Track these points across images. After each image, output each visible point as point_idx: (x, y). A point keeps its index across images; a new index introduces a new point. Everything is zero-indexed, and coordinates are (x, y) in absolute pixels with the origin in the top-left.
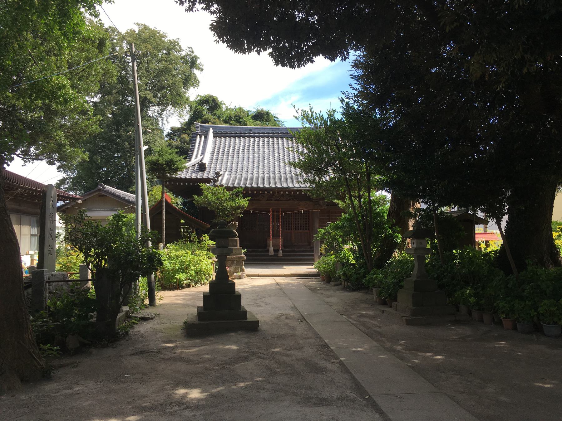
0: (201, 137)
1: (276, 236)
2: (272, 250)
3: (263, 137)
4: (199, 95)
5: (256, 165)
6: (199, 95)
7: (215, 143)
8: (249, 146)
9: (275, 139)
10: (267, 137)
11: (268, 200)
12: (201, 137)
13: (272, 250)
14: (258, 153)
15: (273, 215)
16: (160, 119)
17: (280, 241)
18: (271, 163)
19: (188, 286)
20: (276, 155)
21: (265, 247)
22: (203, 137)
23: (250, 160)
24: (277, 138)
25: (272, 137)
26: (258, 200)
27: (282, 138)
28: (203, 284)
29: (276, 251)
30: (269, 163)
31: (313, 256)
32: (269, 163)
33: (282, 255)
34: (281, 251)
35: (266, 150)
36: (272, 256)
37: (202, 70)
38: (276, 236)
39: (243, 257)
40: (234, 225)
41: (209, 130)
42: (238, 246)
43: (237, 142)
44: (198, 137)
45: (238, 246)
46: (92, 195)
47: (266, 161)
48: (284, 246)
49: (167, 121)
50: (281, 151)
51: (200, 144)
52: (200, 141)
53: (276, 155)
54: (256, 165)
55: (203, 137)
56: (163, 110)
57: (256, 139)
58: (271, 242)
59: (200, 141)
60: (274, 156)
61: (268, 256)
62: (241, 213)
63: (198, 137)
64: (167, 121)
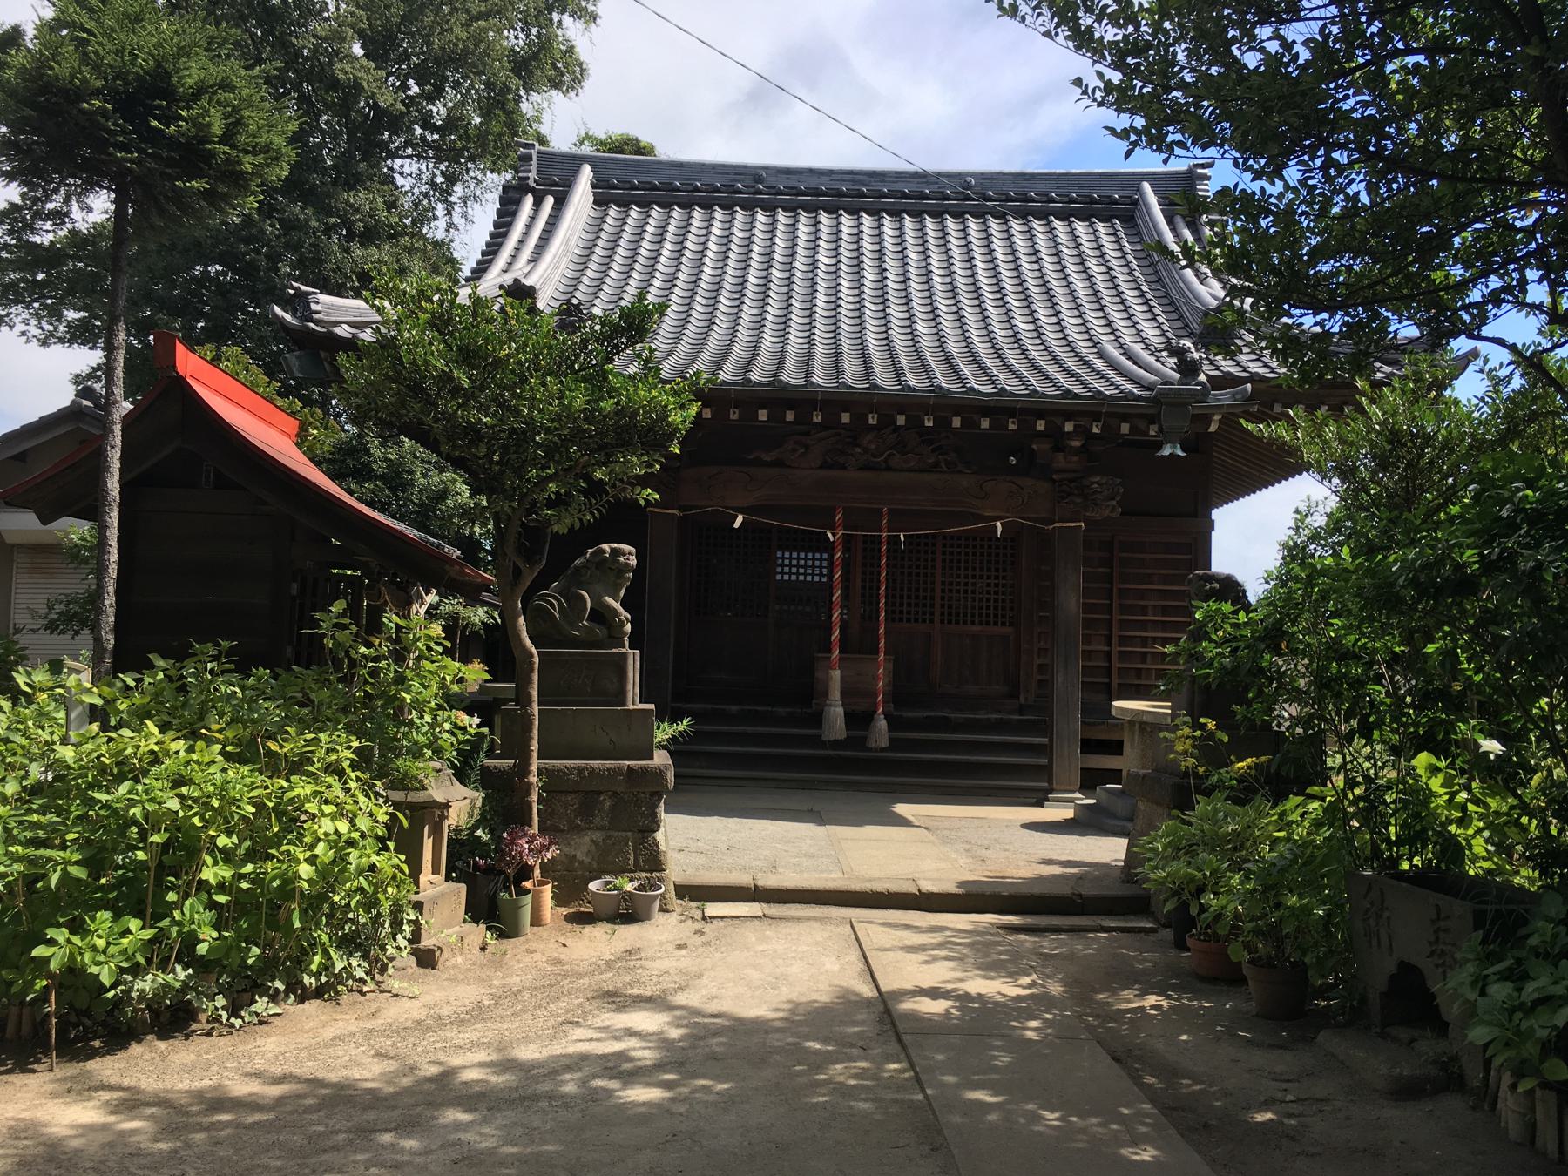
0: (538, 204)
1: (858, 645)
2: (836, 713)
3: (812, 209)
4: (587, 136)
5: (773, 311)
6: (587, 136)
7: (597, 227)
8: (749, 241)
9: (867, 220)
10: (832, 210)
11: (825, 466)
12: (538, 204)
13: (836, 713)
14: (789, 267)
15: (847, 540)
16: (440, 210)
17: (881, 673)
18: (846, 308)
19: (173, 1019)
20: (869, 276)
21: (809, 698)
22: (549, 201)
23: (751, 290)
24: (875, 213)
25: (854, 211)
26: (779, 463)
27: (896, 214)
28: (318, 993)
29: (859, 719)
30: (835, 304)
31: (1045, 750)
32: (835, 304)
33: (885, 743)
34: (882, 723)
35: (824, 259)
36: (836, 744)
37: (593, 17)
38: (858, 645)
39: (658, 774)
40: (609, 569)
41: (576, 172)
42: (633, 702)
43: (696, 223)
44: (529, 200)
45: (633, 702)
46: (50, 436)
47: (821, 299)
48: (898, 696)
49: (464, 215)
50: (890, 263)
51: (529, 226)
52: (533, 218)
53: (869, 276)
54: (773, 311)
55: (549, 201)
56: (451, 180)
57: (783, 218)
58: (836, 674)
59: (533, 218)
60: (858, 284)
61: (817, 741)
62: (644, 481)
63: (529, 200)
64: (464, 215)
